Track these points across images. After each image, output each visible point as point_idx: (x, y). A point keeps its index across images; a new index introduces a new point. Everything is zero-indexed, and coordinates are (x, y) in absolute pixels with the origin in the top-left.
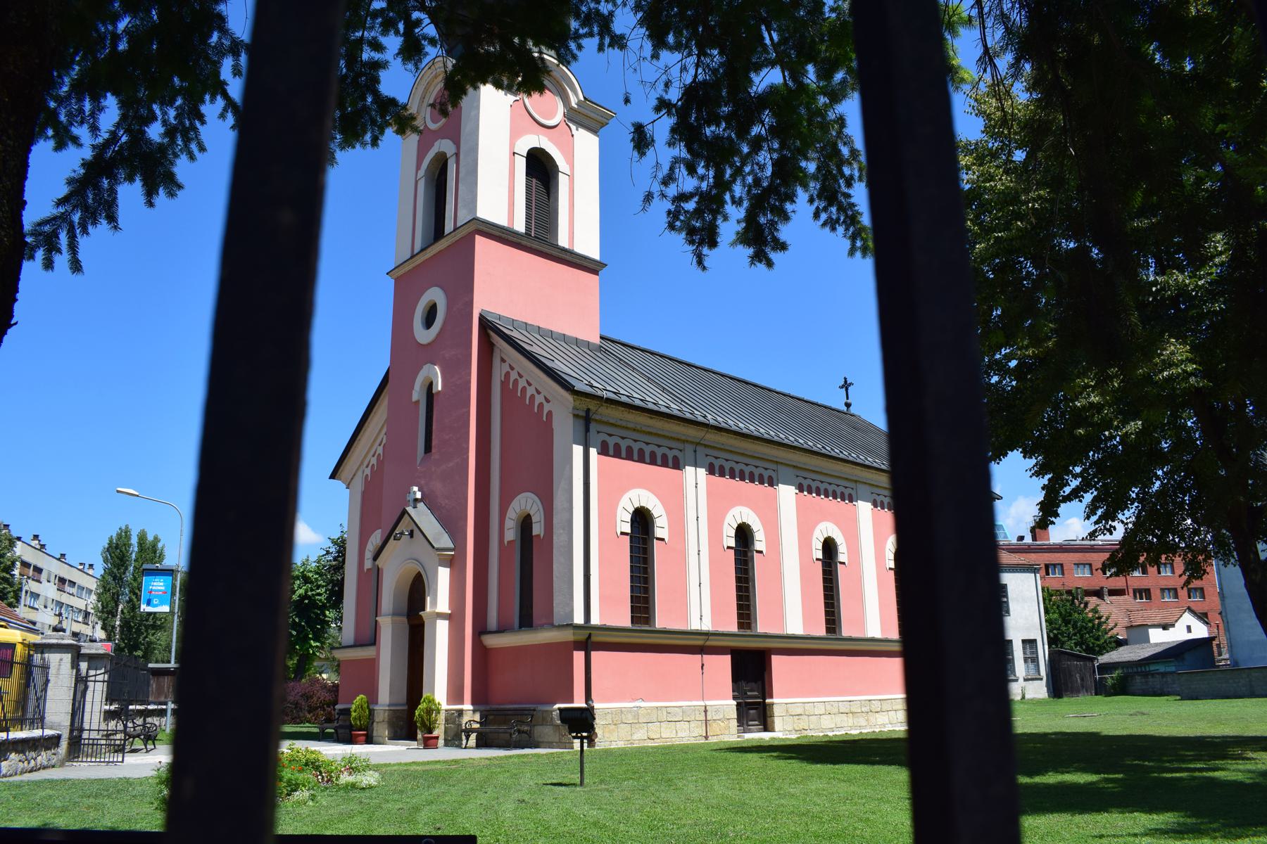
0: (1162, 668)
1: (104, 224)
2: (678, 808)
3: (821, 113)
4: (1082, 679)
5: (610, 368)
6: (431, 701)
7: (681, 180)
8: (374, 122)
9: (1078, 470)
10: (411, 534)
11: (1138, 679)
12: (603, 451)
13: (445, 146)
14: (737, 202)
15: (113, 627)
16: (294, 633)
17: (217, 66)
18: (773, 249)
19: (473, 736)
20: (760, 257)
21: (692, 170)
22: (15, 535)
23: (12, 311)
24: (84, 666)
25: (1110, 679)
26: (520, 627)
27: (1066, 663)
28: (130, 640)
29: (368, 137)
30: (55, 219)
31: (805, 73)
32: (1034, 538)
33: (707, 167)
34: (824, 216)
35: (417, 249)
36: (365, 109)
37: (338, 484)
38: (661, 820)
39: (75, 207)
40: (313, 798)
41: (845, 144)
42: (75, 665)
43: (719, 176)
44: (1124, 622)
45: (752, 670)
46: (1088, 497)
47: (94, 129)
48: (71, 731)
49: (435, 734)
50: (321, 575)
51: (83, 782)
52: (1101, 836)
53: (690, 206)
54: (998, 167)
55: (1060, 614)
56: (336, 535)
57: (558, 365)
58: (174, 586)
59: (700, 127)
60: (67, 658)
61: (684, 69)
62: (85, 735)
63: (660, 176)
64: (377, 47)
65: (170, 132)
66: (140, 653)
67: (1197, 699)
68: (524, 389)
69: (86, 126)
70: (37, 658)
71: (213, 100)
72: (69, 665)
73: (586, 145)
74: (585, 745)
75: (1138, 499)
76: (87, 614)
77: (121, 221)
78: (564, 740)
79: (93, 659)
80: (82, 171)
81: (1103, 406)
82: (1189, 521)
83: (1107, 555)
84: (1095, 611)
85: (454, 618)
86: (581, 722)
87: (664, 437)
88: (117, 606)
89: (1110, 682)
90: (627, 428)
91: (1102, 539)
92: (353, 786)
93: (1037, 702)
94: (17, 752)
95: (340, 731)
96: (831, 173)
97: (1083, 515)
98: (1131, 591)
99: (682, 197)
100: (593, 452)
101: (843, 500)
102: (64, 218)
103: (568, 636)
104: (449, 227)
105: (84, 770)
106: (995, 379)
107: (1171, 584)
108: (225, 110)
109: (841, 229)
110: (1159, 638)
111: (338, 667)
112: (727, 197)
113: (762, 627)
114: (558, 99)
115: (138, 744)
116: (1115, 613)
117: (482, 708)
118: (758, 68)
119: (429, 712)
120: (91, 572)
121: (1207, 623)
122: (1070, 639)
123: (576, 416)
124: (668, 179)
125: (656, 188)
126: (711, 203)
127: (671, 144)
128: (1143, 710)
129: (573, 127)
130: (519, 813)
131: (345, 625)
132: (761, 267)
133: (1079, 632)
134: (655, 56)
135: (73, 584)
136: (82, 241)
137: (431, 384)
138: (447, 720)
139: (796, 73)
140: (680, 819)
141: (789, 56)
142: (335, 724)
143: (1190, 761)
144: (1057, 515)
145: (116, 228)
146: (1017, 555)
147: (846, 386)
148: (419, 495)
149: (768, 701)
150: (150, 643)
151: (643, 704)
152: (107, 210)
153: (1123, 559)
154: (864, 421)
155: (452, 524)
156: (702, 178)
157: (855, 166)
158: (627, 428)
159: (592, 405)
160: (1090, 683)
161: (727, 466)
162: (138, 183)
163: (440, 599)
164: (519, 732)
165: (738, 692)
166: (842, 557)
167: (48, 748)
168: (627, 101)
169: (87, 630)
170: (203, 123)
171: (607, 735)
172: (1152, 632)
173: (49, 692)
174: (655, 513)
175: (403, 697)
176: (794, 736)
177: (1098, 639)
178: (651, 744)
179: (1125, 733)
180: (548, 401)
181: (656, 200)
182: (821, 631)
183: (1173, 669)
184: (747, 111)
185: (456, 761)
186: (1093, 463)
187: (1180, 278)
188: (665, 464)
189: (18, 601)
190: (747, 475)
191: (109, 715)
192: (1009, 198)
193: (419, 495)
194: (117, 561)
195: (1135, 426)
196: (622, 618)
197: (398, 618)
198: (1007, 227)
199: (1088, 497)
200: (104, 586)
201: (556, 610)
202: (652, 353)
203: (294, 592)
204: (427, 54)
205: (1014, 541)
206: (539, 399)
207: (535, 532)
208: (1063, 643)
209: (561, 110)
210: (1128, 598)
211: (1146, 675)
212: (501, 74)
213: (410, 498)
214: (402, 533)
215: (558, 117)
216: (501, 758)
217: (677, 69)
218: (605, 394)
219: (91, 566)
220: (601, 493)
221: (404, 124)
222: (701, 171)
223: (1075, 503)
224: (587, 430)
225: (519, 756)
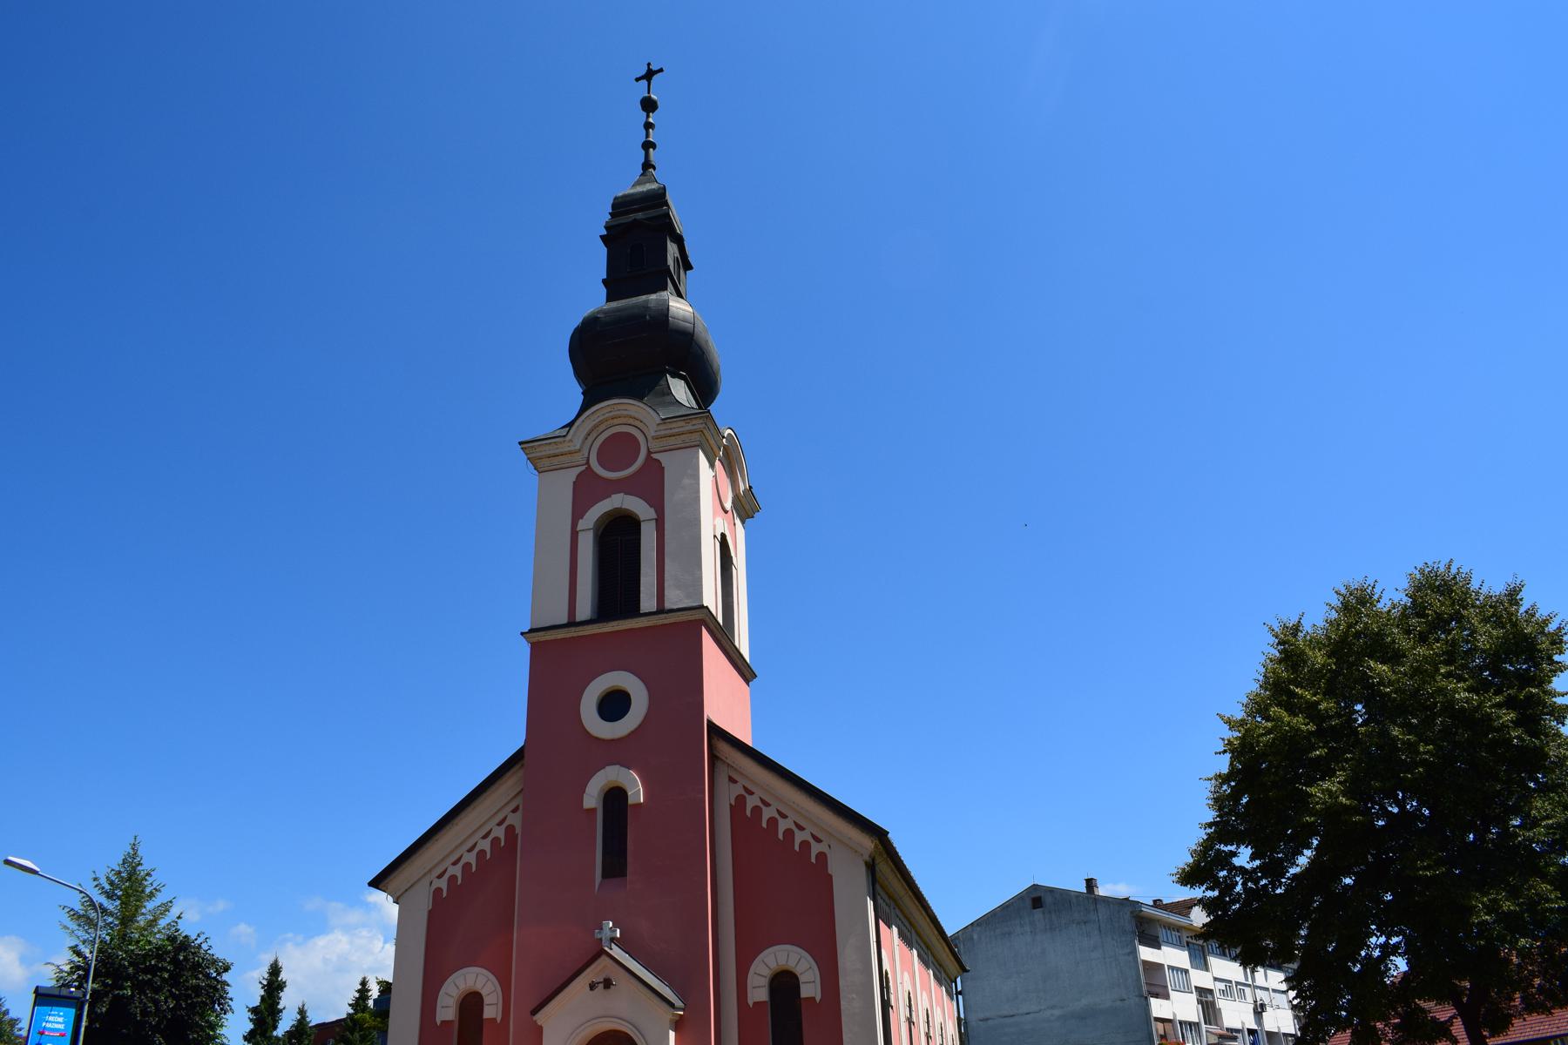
13: (637, 506)
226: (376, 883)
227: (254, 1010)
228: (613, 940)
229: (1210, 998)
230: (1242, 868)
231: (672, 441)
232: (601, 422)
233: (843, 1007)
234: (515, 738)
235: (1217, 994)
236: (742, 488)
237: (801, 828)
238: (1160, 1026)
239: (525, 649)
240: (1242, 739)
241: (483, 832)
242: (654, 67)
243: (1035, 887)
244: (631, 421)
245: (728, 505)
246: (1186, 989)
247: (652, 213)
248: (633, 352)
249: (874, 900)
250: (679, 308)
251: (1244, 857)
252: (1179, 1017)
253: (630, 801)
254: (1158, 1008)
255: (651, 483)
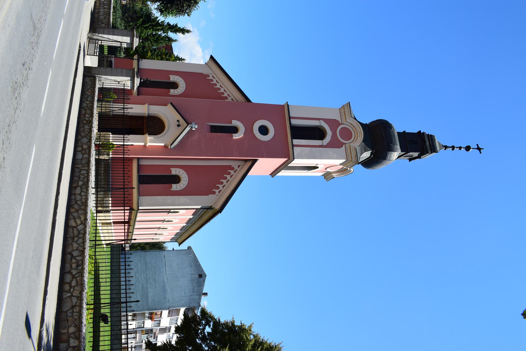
226: (212, 57)
227: (176, 25)
228: (192, 127)
229: (167, 331)
230: (205, 328)
231: (349, 151)
232: (356, 129)
233: (170, 197)
234: (254, 99)
235: (169, 333)
236: (334, 175)
237: (223, 187)
238: (160, 313)
239: (282, 103)
240: (245, 329)
241: (230, 94)
242: (482, 151)
243: (205, 276)
244: (356, 138)
245: (328, 170)
246: (171, 323)
247: (428, 148)
248: (379, 140)
249: (201, 208)
250: (395, 155)
251: (208, 330)
252: (162, 320)
253: (234, 134)
254: (165, 313)
255: (335, 144)
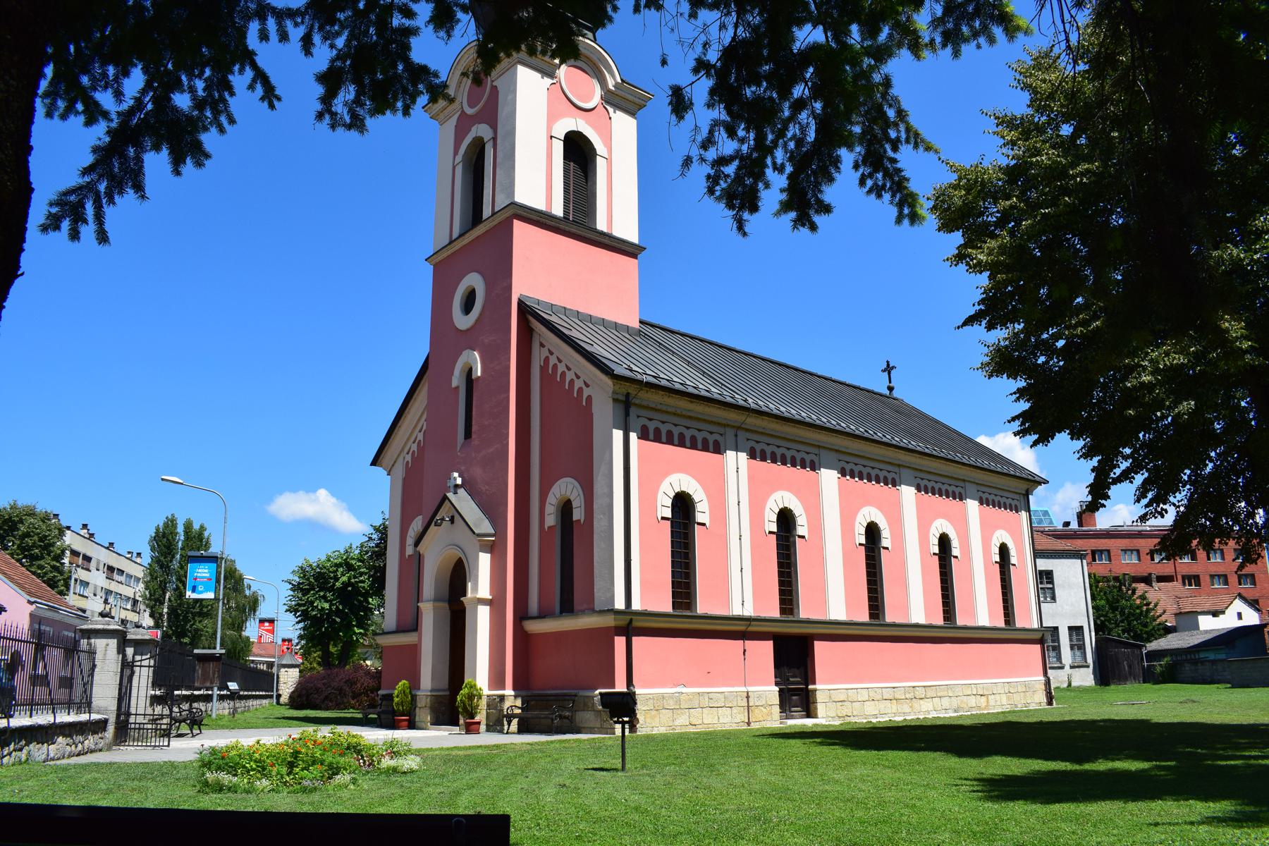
0: (1212, 656)
1: (130, 194)
2: (721, 794)
3: (866, 75)
4: (1130, 667)
5: (650, 353)
6: (473, 686)
7: (720, 143)
8: (405, 91)
9: (1128, 451)
10: (452, 520)
11: (1187, 667)
12: (644, 436)
13: (482, 130)
14: (779, 169)
15: (161, 615)
16: (338, 620)
17: (243, 34)
18: (818, 212)
19: (515, 721)
20: (804, 220)
21: (732, 133)
22: (64, 524)
23: (19, 262)
24: (130, 651)
25: (1159, 666)
26: (561, 612)
27: (1114, 651)
28: (177, 627)
29: (399, 104)
30: (80, 188)
31: (848, 33)
32: (1080, 524)
33: (747, 130)
34: (869, 183)
35: (455, 235)
36: (397, 77)
37: (380, 472)
38: (703, 805)
39: (101, 176)
40: (354, 781)
41: (890, 106)
42: (121, 650)
43: (760, 138)
44: (1172, 608)
45: (794, 656)
46: (1139, 479)
47: (119, 95)
48: (118, 716)
49: (477, 719)
50: (362, 561)
51: (129, 765)
52: (1156, 824)
53: (730, 169)
54: (1044, 142)
55: (1107, 600)
56: (378, 523)
57: (597, 350)
58: (218, 574)
59: (740, 88)
60: (113, 643)
61: (723, 27)
62: (132, 719)
63: (699, 139)
64: (409, 14)
65: (199, 104)
66: (186, 640)
67: (1248, 686)
68: (563, 374)
69: (110, 91)
70: (84, 642)
71: (241, 71)
72: (115, 651)
73: (624, 127)
74: (627, 731)
75: (1190, 481)
76: (135, 602)
77: (148, 190)
78: (606, 725)
79: (140, 645)
80: (108, 139)
81: (1155, 385)
82: (1243, 504)
83: (1157, 540)
84: (1143, 597)
85: (496, 604)
86: (623, 707)
87: (705, 421)
88: (164, 594)
89: (1158, 669)
90: (667, 412)
91: (1155, 522)
92: (395, 770)
93: (1082, 690)
94: (65, 736)
95: (383, 716)
96: (875, 136)
97: (1133, 498)
98: (1180, 578)
99: (722, 161)
100: (633, 436)
101: (886, 484)
102: (89, 188)
103: (609, 621)
104: (487, 212)
105: (130, 754)
106: (1042, 359)
107: (1221, 570)
108: (254, 81)
109: (887, 196)
110: (1208, 624)
111: (381, 653)
112: (769, 161)
113: (805, 612)
114: (595, 82)
115: (184, 729)
116: (1163, 599)
117: (524, 693)
118: (800, 23)
119: (471, 697)
120: (138, 560)
121: (1258, 610)
122: (1118, 626)
123: (615, 400)
124: (708, 143)
125: (695, 152)
126: (753, 167)
127: (710, 105)
128: (1194, 698)
129: (611, 110)
130: (560, 797)
131: (387, 612)
132: (805, 231)
133: (1127, 618)
134: (693, 15)
135: (121, 572)
136: (109, 211)
137: (471, 369)
138: (488, 705)
139: (839, 32)
140: (723, 804)
141: (831, 16)
142: (378, 709)
143: (1245, 749)
144: (1107, 497)
145: (143, 197)
146: (1063, 541)
147: (889, 369)
148: (459, 481)
149: (810, 687)
150: (197, 630)
151: (684, 690)
152: (133, 179)
153: (1174, 543)
154: (907, 405)
155: (493, 510)
156: (742, 141)
157: (902, 127)
158: (667, 412)
159: (632, 390)
160: (1138, 670)
161: (769, 450)
162: (165, 152)
163: (481, 585)
164: (561, 717)
165: (780, 678)
166: (886, 542)
167: (95, 732)
168: (664, 62)
169: (133, 617)
170: (232, 94)
171: (648, 720)
172: (1201, 619)
173: (96, 677)
174: (696, 498)
175: (445, 683)
176: (837, 723)
177: (1145, 625)
178: (692, 729)
179: (1176, 720)
180: (587, 386)
181: (695, 164)
182: (864, 617)
183: (1223, 656)
184: (789, 68)
185: (498, 746)
186: (1144, 445)
187: (1235, 252)
188: (705, 448)
189: (68, 588)
190: (789, 460)
191: (155, 700)
192: (1055, 173)
193: (459, 481)
194: (165, 550)
195: (1188, 405)
196: (666, 606)
197: (441, 604)
198: (1053, 203)
199: (1139, 479)
200: (151, 572)
201: (596, 595)
202: (692, 337)
203: (337, 579)
204: (459, 21)
205: (1060, 527)
206: (578, 384)
207: (575, 518)
208: (1111, 630)
209: (598, 92)
210: (1176, 585)
211: (1195, 662)
212: (534, 39)
213: (451, 484)
214: (443, 519)
215: (596, 100)
216: (543, 743)
217: (717, 30)
218: (645, 378)
219: (139, 554)
220: (642, 478)
221: (438, 92)
222: (741, 133)
223: (1126, 484)
224: (627, 414)
225: (560, 741)
